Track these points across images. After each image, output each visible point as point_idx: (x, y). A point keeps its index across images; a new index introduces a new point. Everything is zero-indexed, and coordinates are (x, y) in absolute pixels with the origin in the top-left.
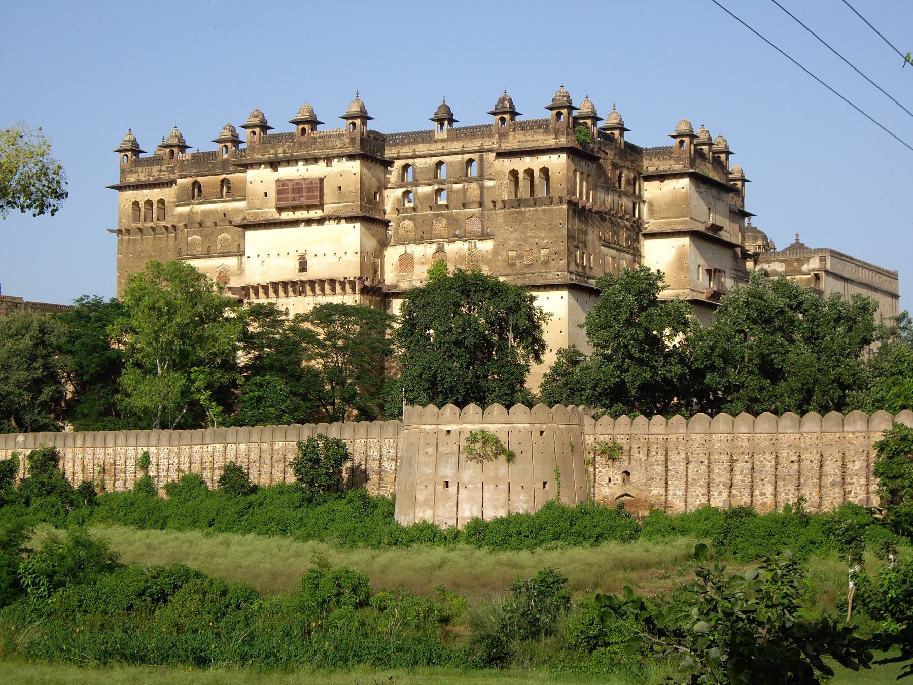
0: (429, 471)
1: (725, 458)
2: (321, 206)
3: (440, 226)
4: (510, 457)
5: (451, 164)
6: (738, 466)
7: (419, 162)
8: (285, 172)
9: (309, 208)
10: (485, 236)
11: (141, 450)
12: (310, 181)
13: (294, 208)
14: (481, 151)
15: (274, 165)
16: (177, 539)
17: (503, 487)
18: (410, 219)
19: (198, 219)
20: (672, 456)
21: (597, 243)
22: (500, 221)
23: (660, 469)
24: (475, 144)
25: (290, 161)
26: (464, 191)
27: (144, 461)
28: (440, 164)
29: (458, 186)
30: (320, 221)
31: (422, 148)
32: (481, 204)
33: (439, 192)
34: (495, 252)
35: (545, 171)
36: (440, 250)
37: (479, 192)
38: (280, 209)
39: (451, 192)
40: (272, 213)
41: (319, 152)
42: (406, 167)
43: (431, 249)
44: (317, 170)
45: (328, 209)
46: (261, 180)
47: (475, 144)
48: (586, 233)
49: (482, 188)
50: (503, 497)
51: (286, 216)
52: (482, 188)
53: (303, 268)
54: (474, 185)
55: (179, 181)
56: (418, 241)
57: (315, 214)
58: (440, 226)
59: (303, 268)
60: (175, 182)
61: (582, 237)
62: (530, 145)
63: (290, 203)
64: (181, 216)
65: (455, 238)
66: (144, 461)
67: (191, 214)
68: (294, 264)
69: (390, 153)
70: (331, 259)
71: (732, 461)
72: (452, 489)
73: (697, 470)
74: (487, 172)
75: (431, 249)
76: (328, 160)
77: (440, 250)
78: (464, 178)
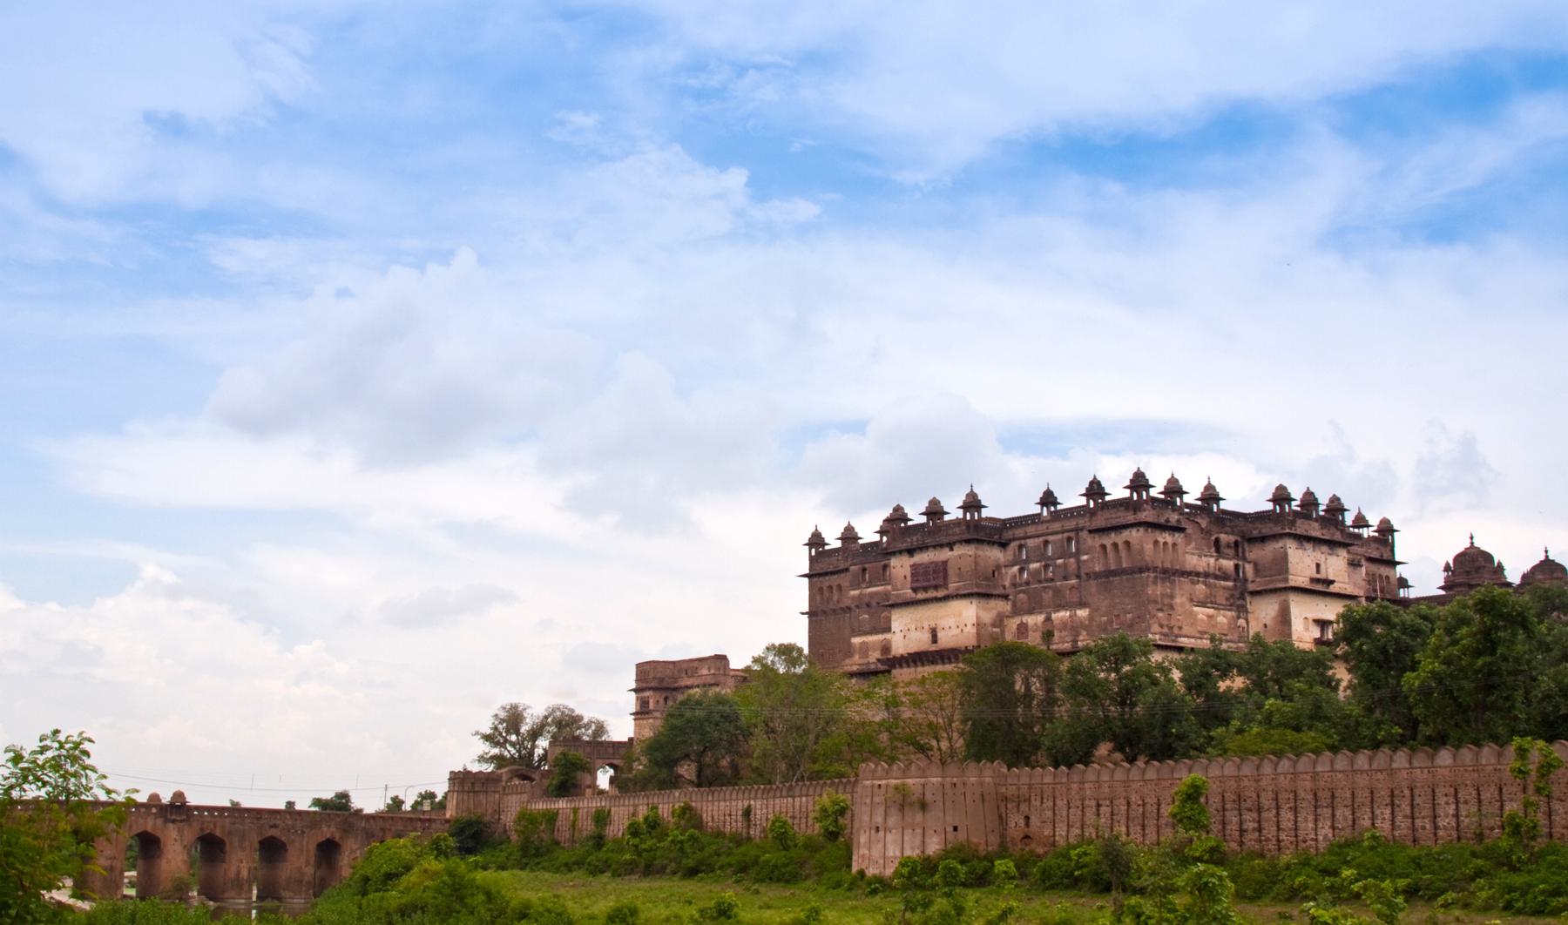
0: (866, 818)
1: (1093, 803)
2: (945, 586)
3: (1048, 596)
4: (924, 806)
5: (1054, 543)
6: (1103, 809)
7: (1030, 543)
8: (922, 558)
9: (936, 587)
10: (1082, 605)
11: (746, 804)
12: (936, 563)
13: (925, 589)
14: (1077, 530)
15: (910, 552)
16: (661, 888)
17: (919, 831)
18: (1024, 592)
19: (866, 600)
20: (1058, 802)
21: (1188, 606)
22: (1094, 590)
23: (1049, 813)
24: (1071, 524)
25: (923, 548)
26: (1065, 565)
27: (747, 813)
28: (1046, 543)
29: (1060, 561)
30: (946, 598)
31: (1031, 530)
32: (1078, 576)
33: (1046, 567)
34: (1091, 618)
35: (1127, 543)
36: (1048, 619)
37: (1188, 568)
38: (915, 590)
39: (1056, 566)
40: (908, 593)
41: (944, 540)
42: (1020, 547)
43: (1041, 618)
44: (944, 554)
45: (952, 587)
46: (901, 566)
47: (1071, 524)
48: (1172, 597)
49: (1078, 561)
50: (918, 841)
51: (921, 596)
52: (1078, 561)
53: (935, 640)
54: (1072, 560)
55: (852, 568)
56: (1031, 612)
57: (940, 594)
58: (1048, 596)
59: (935, 640)
60: (847, 570)
61: (1166, 601)
62: (1114, 522)
63: (933, 582)
64: (854, 598)
65: (1060, 607)
66: (747, 813)
67: (860, 597)
68: (927, 636)
69: (1008, 535)
70: (956, 631)
71: (1099, 806)
72: (881, 833)
73: (1075, 814)
74: (1082, 547)
75: (1041, 618)
76: (951, 546)
77: (1048, 619)
78: (1065, 554)
